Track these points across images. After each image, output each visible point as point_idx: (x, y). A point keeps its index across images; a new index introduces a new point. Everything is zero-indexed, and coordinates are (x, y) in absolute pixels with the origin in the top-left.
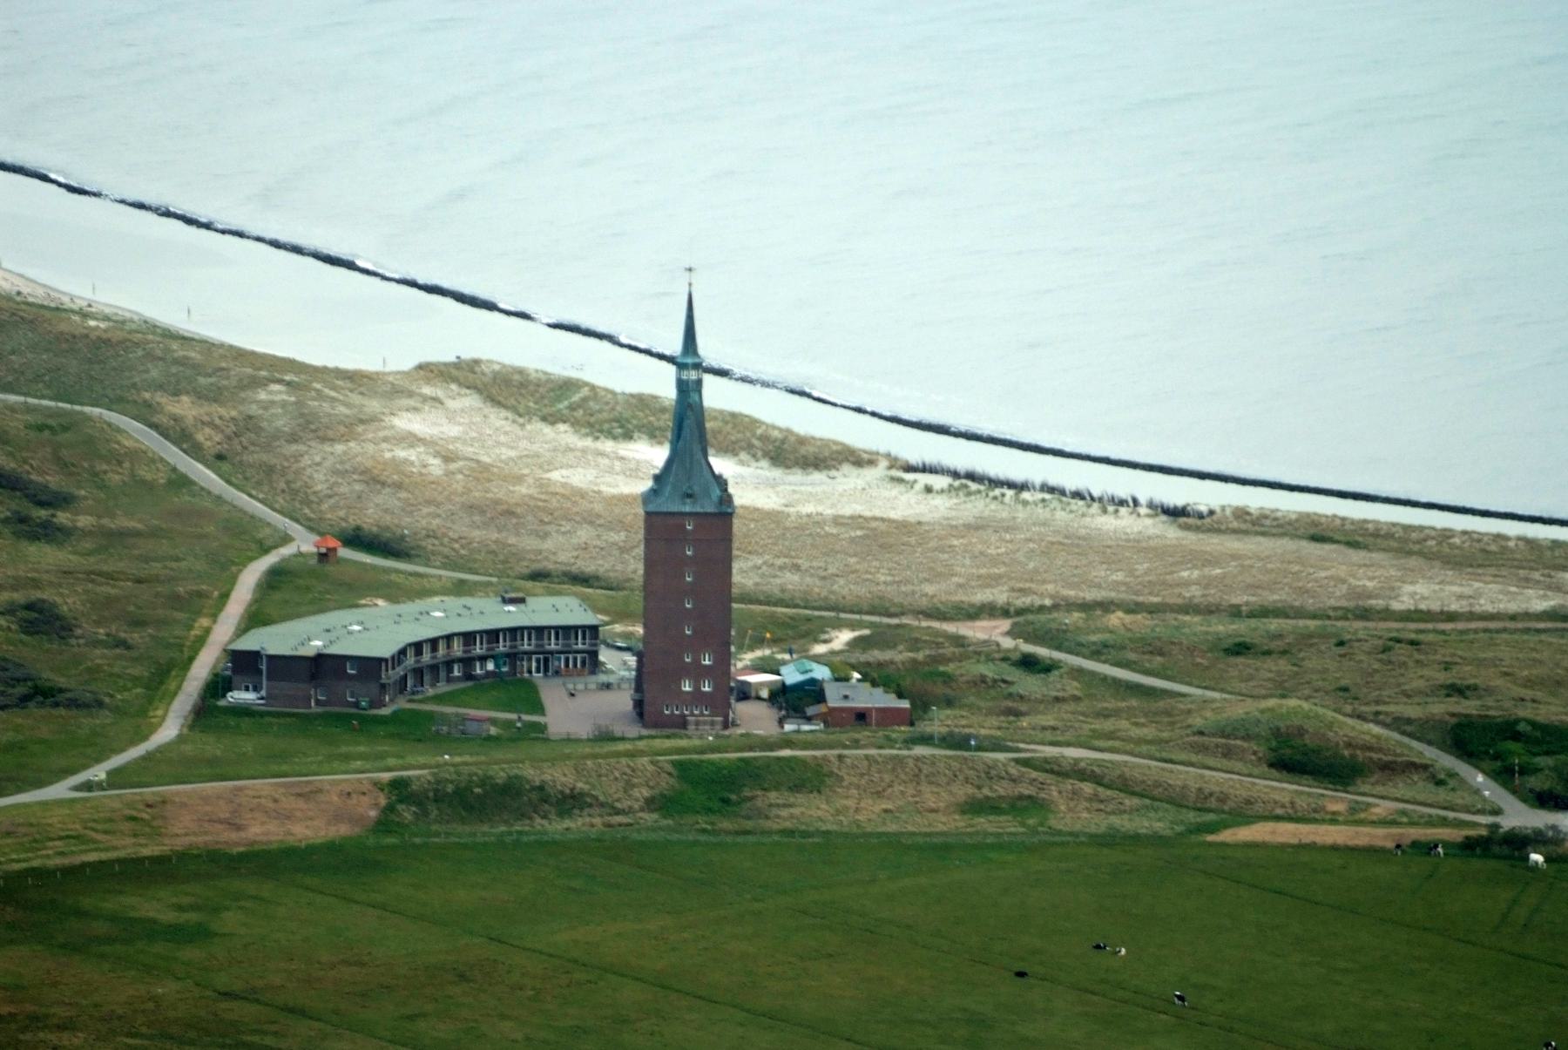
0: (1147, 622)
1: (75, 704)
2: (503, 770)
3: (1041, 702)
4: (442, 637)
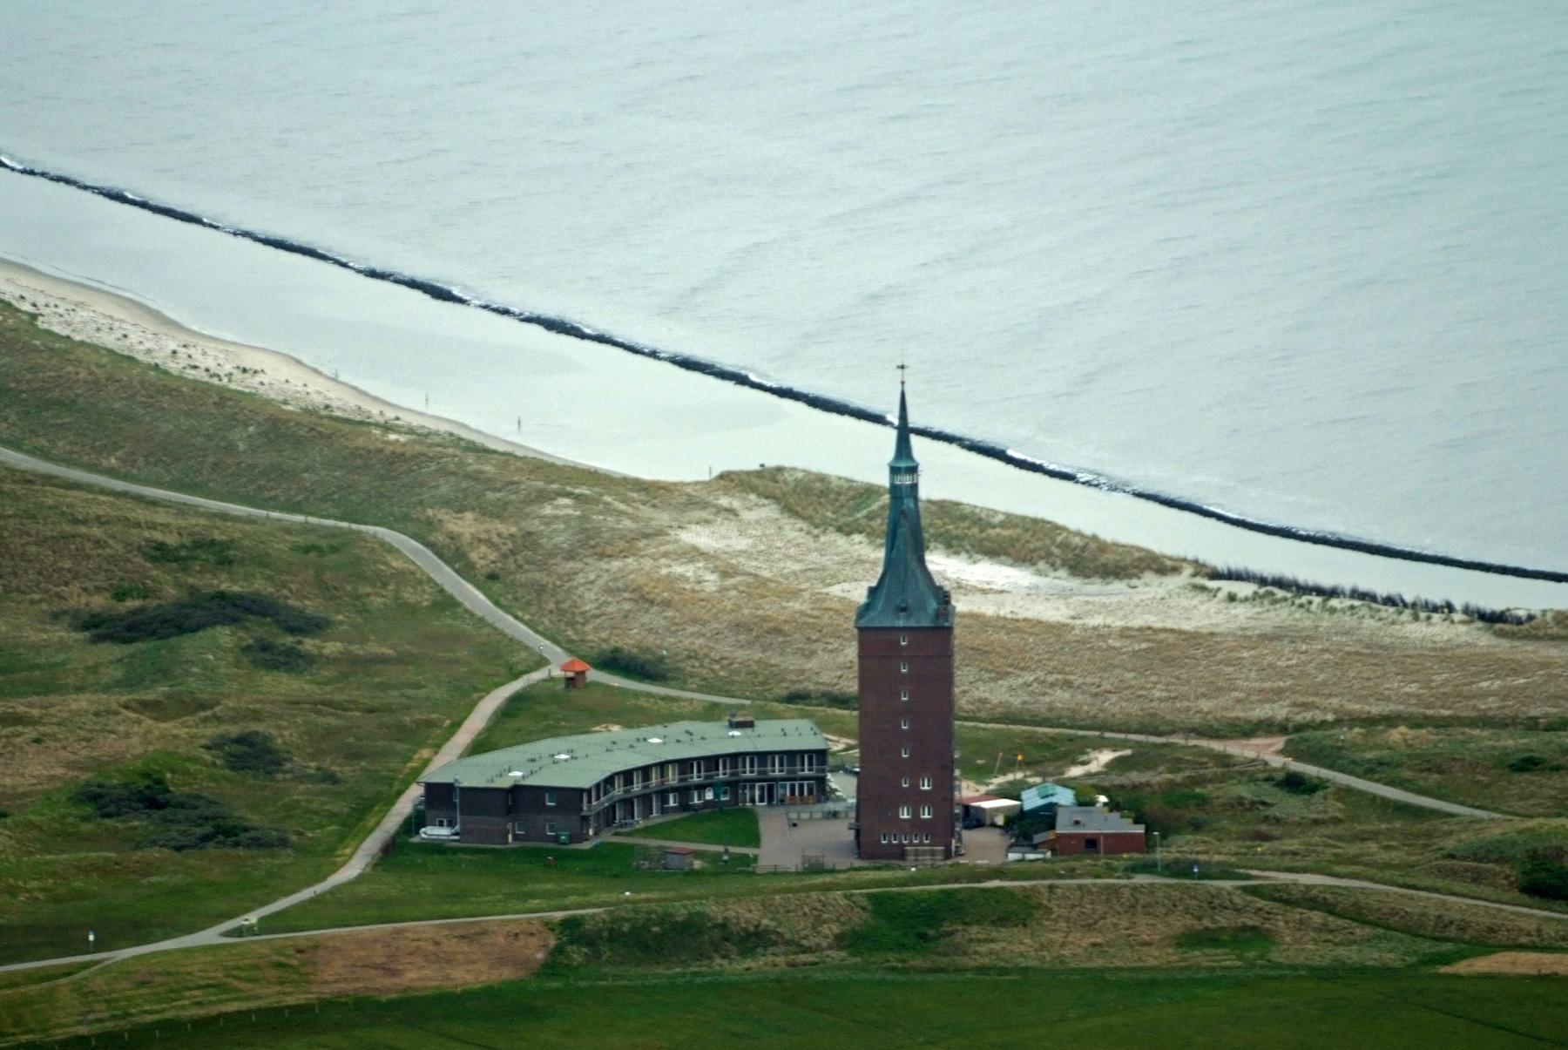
0: (1432, 737)
1: (258, 843)
2: (684, 906)
3: (1299, 824)
4: (655, 765)
